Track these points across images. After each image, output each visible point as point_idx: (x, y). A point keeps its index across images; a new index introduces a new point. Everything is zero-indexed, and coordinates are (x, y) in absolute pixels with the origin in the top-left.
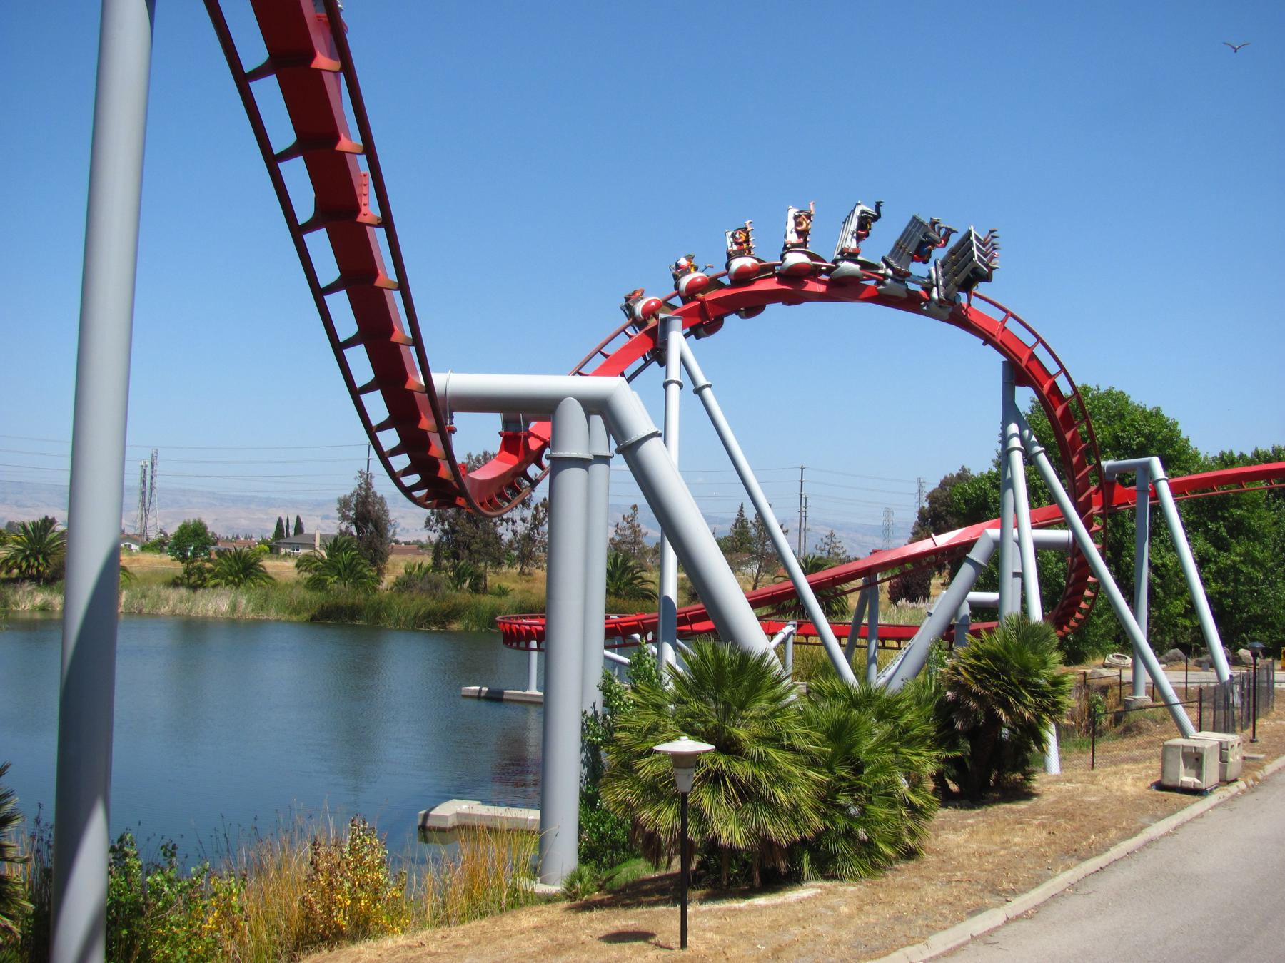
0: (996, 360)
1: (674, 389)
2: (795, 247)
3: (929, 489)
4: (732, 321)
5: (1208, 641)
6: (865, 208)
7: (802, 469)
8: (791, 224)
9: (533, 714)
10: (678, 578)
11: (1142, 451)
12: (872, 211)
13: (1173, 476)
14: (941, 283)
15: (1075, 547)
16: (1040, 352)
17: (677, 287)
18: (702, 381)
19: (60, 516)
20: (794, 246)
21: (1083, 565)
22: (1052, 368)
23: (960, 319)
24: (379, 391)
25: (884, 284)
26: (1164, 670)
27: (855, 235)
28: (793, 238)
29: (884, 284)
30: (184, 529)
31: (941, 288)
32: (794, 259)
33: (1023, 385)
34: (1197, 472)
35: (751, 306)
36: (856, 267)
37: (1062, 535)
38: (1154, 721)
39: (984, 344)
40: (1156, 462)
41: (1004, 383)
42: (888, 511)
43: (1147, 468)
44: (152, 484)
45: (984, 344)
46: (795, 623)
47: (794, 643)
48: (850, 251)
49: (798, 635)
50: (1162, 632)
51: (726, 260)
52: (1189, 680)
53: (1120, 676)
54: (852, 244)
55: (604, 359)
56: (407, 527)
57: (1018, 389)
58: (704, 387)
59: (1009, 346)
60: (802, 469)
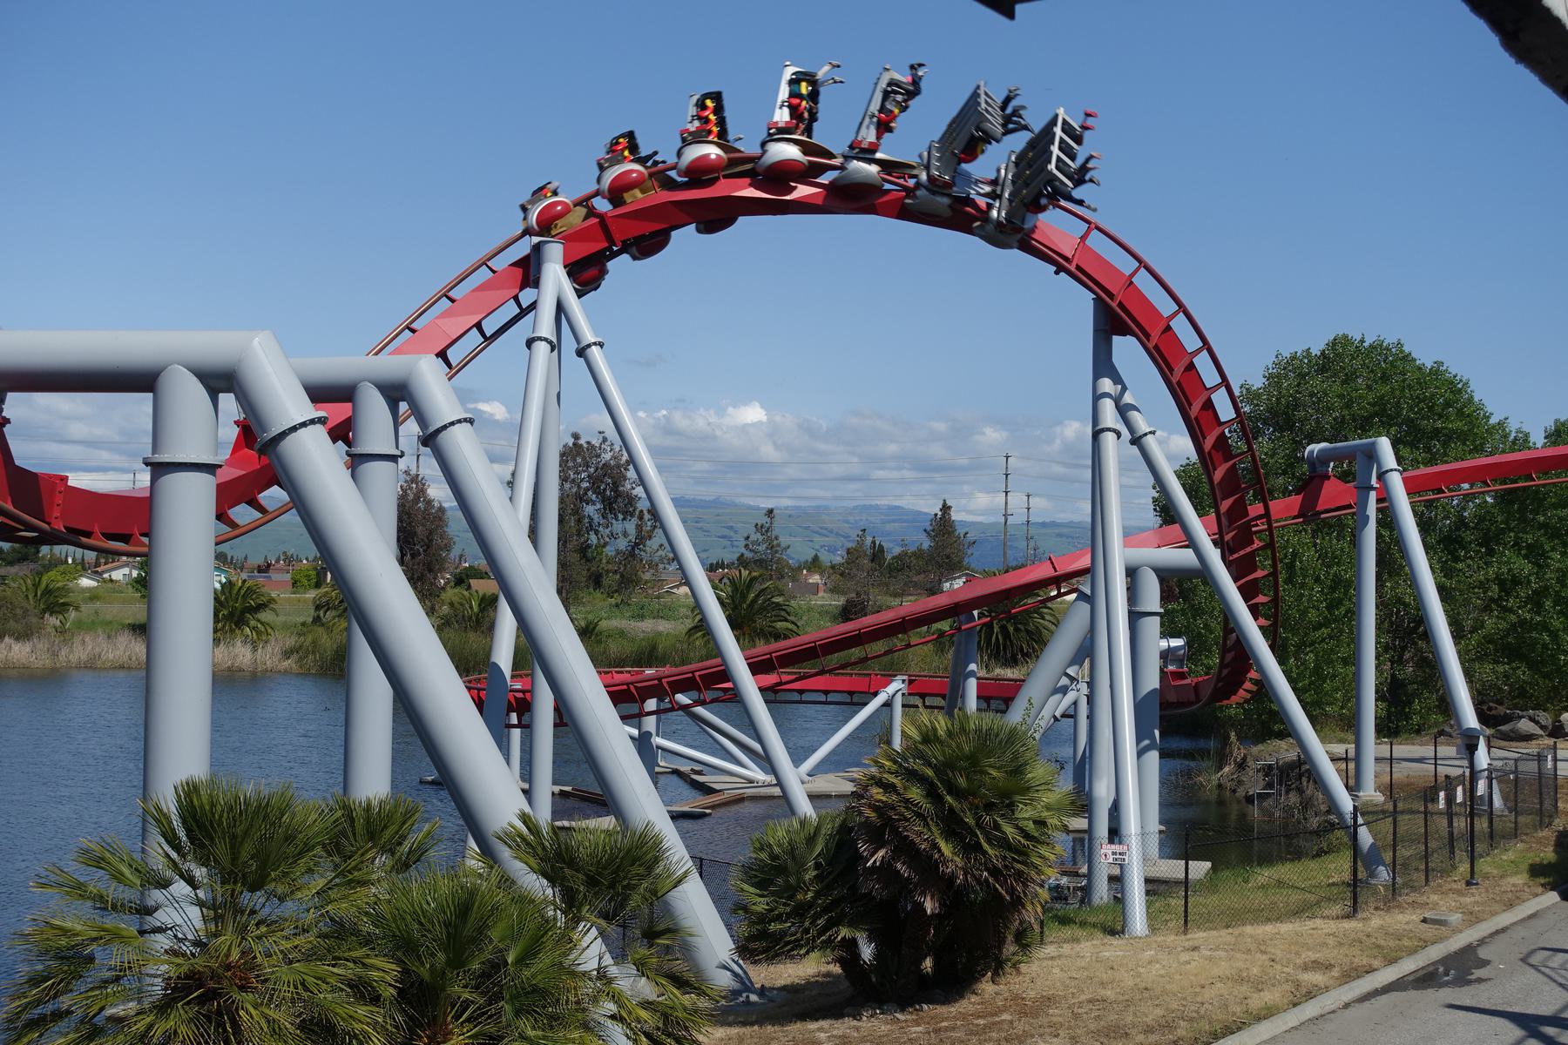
0: (1084, 301)
1: (542, 348)
2: (779, 133)
4: (685, 238)
5: (1455, 708)
6: (898, 77)
8: (784, 92)
9: (1321, 978)
10: (1238, 588)
11: (1365, 426)
12: (904, 78)
13: (1415, 463)
14: (1007, 195)
15: (1203, 574)
17: (679, 154)
18: (589, 336)
20: (781, 131)
23: (1027, 246)
25: (914, 197)
27: (875, 120)
28: (782, 116)
29: (914, 197)
31: (1005, 203)
32: (787, 151)
33: (1123, 334)
34: (1491, 454)
35: (716, 217)
36: (874, 169)
37: (1186, 557)
40: (1385, 445)
41: (1096, 331)
43: (1371, 455)
46: (905, 677)
47: (903, 706)
48: (865, 145)
49: (909, 694)
51: (522, 215)
52: (1433, 766)
54: (869, 135)
57: (1116, 339)
58: (589, 346)
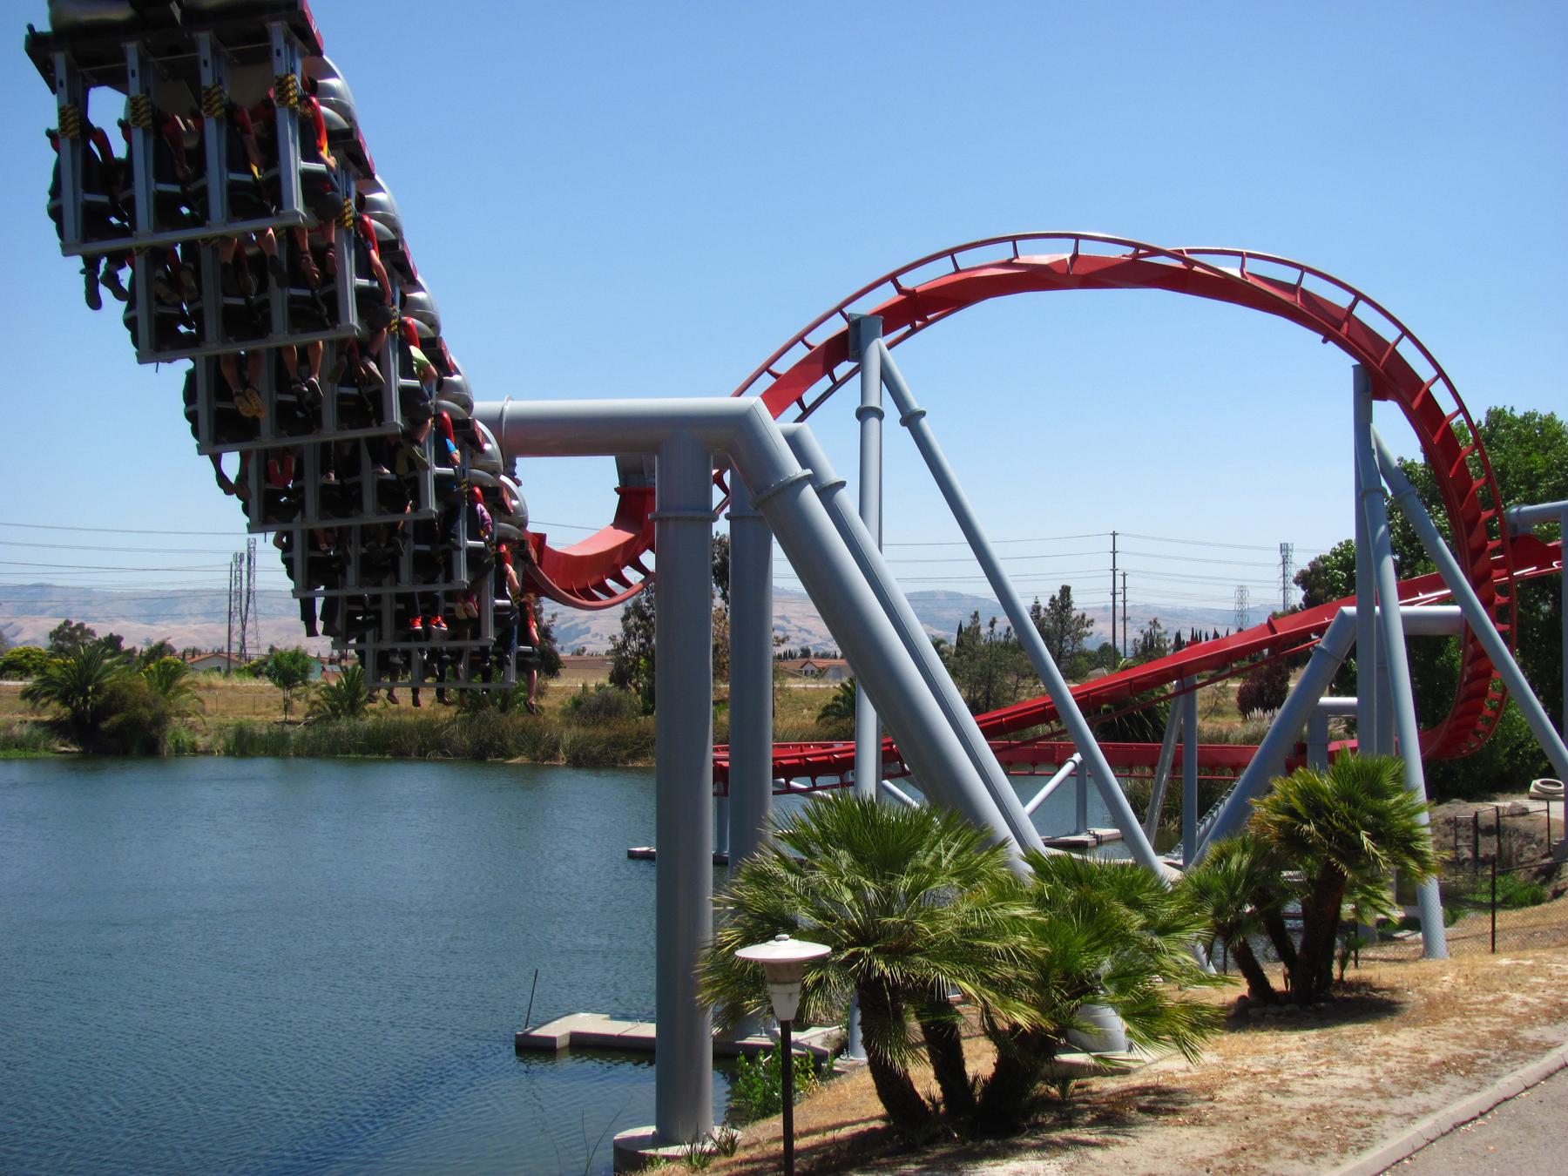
0: (1340, 366)
3: (1302, 561)
7: (1114, 534)
16: (1407, 350)
19: (1110, 642)
21: (1480, 657)
22: (1425, 372)
24: (614, 457)
26: (714, 1107)
30: (56, 635)
33: (1383, 397)
38: (1142, 1110)
39: (1325, 341)
42: (1242, 590)
44: (249, 585)
45: (1325, 341)
50: (754, 939)
53: (1548, 811)
55: (774, 380)
56: (600, 633)
57: (1376, 404)
59: (1356, 339)
60: (1114, 534)
